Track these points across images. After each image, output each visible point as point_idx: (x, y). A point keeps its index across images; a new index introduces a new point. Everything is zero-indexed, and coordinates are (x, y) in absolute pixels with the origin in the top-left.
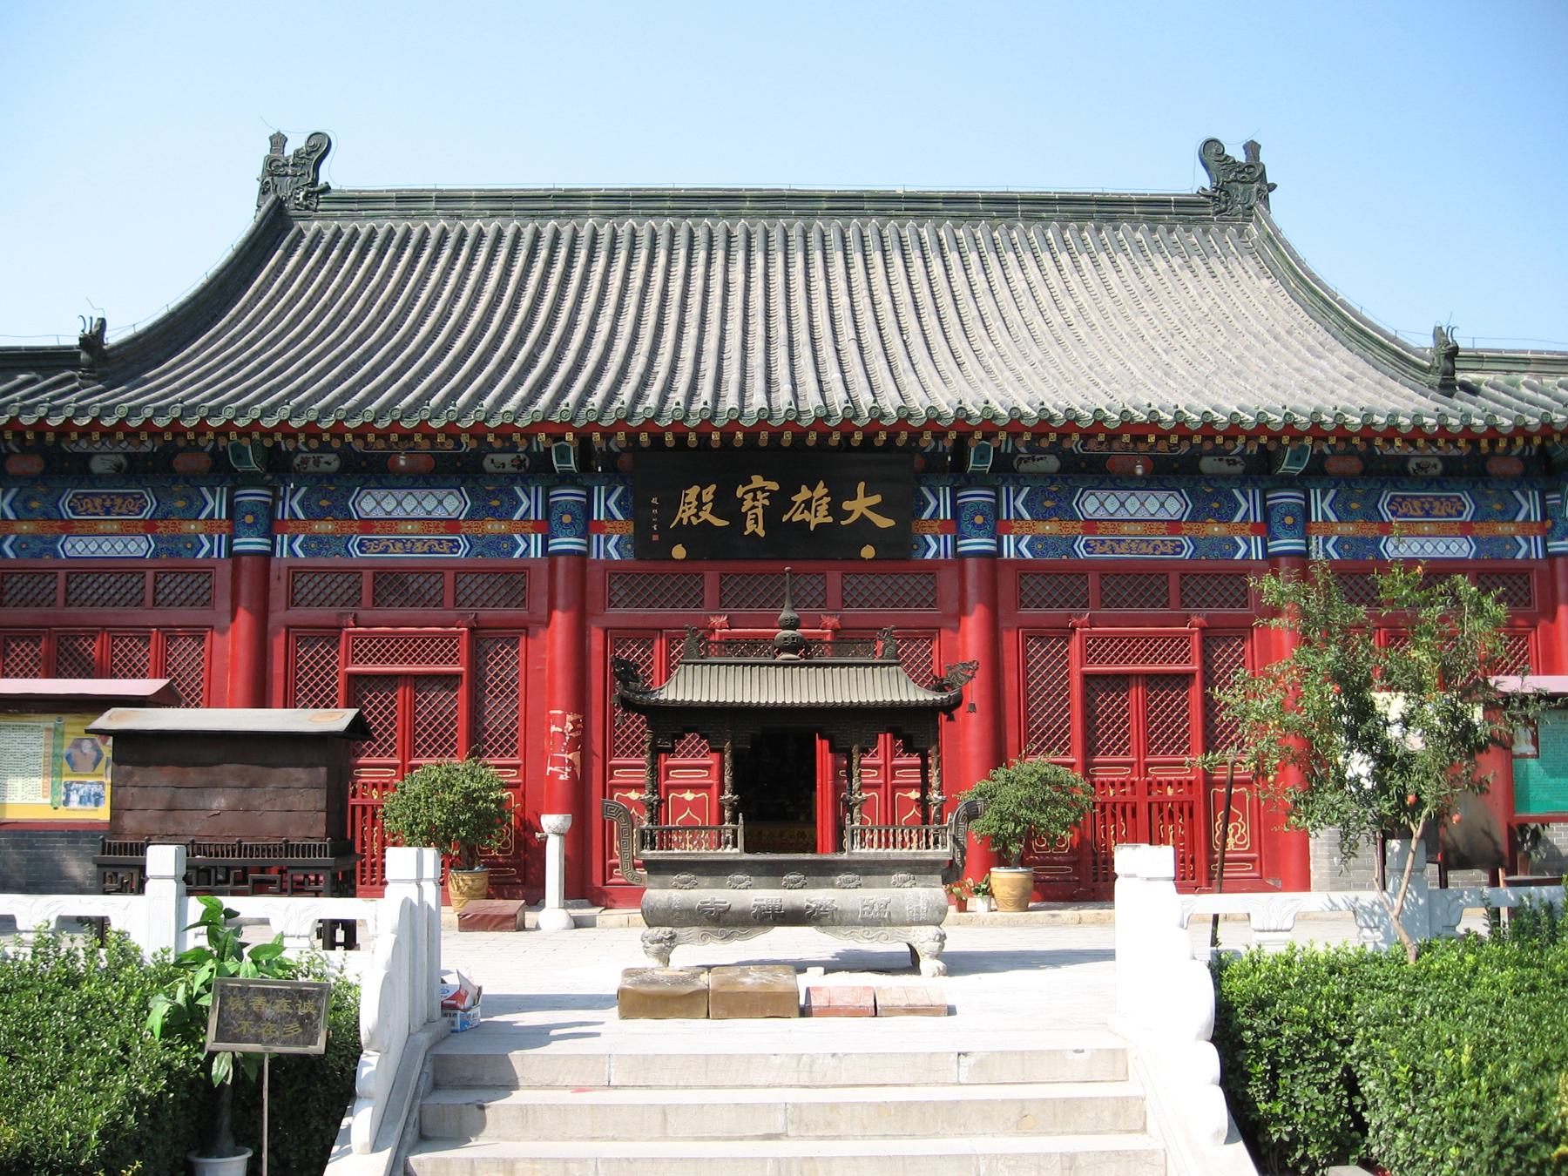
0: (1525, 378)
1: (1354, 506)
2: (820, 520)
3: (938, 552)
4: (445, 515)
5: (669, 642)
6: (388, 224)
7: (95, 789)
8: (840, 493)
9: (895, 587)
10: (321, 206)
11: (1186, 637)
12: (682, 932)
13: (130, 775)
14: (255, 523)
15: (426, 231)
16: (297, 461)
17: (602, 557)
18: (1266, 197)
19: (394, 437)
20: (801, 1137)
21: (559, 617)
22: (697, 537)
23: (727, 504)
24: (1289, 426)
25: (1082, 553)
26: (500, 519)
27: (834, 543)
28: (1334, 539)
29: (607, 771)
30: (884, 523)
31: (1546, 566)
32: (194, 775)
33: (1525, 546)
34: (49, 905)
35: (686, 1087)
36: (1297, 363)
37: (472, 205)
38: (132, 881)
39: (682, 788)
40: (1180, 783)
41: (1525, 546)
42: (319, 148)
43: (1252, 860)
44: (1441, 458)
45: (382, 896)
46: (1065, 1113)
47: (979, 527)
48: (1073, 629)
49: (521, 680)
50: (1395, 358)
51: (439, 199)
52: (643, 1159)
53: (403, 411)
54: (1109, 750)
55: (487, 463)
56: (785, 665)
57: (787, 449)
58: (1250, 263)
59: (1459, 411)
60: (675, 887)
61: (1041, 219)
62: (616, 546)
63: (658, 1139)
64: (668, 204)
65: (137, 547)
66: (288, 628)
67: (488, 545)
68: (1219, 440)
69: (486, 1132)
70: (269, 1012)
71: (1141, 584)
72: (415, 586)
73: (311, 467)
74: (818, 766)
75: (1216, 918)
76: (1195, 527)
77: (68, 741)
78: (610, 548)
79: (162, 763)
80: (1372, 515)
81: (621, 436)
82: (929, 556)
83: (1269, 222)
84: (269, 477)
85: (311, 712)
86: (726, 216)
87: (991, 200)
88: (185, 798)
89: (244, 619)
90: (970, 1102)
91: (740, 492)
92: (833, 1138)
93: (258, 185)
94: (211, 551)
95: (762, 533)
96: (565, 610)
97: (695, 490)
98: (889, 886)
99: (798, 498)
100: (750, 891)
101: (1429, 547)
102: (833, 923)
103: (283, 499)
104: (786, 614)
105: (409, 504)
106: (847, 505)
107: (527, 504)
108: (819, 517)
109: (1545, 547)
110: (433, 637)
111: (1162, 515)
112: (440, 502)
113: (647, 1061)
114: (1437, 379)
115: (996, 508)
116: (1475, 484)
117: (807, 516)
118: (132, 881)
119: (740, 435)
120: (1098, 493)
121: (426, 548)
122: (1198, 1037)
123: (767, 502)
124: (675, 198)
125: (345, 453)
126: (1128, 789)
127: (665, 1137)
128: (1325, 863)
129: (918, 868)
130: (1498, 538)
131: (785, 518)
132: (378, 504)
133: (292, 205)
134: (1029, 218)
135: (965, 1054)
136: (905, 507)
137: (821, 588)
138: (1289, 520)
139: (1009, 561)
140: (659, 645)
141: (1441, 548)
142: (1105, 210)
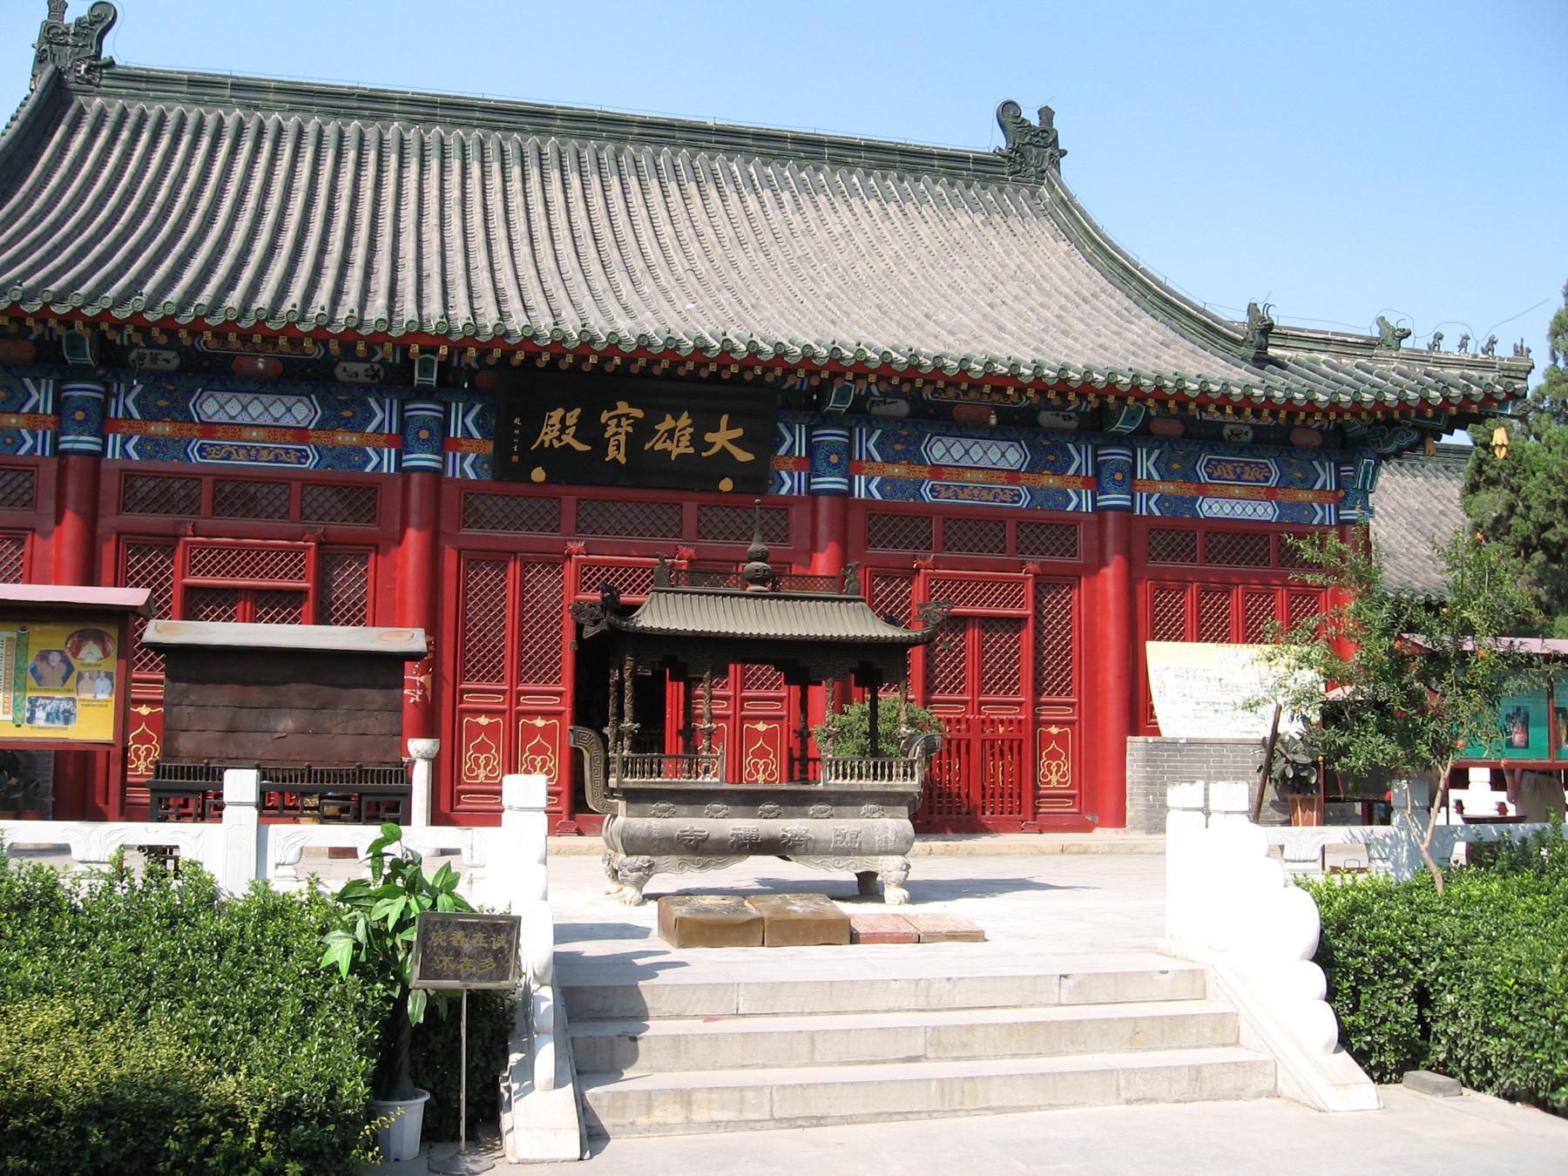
0: (1323, 357)
1: (1175, 466)
2: (682, 450)
3: (792, 488)
4: (293, 423)
5: (523, 565)
6: (179, 108)
7: (64, 705)
8: (704, 423)
9: (531, 511)
10: (104, 82)
11: (1020, 582)
12: (660, 860)
13: (186, 693)
14: (86, 420)
15: (221, 120)
16: (133, 355)
17: (458, 475)
19: (257, 338)
20: (939, 1059)
21: (412, 534)
22: (559, 462)
23: (590, 430)
24: (1136, 388)
25: (928, 497)
26: (352, 430)
27: (697, 474)
28: (1156, 496)
29: (458, 695)
30: (744, 456)
31: (1094, 518)
32: (257, 694)
33: (1320, 513)
34: (110, 833)
35: (811, 1014)
36: (1114, 328)
37: (271, 96)
38: (209, 808)
39: (534, 714)
40: (1011, 722)
41: (1320, 513)
43: (1072, 797)
44: (1252, 426)
45: (499, 824)
46: (1170, 1030)
48: (918, 570)
49: (369, 599)
50: (1208, 331)
52: (816, 1085)
53: (55, 294)
54: (946, 688)
55: (339, 371)
56: (756, 597)
57: (515, 368)
58: (1048, 224)
59: (1279, 385)
60: (653, 815)
61: (846, 164)
62: (473, 465)
63: (806, 1065)
64: (478, 115)
65: (1264, 511)
66: (119, 534)
67: (338, 457)
68: (895, 381)
69: (638, 1063)
70: (467, 947)
71: (885, 524)
72: (145, 489)
73: (147, 364)
74: (668, 696)
75: (1323, 848)
76: (1032, 477)
77: (33, 654)
78: (466, 467)
79: (222, 681)
80: (1190, 476)
81: (472, 352)
82: (784, 491)
83: (1062, 186)
84: (101, 372)
85: (285, 627)
86: (537, 133)
87: (800, 140)
88: (247, 718)
89: (70, 520)
90: (1090, 1021)
91: (604, 417)
92: (968, 1058)
93: (33, 52)
94: (34, 448)
95: (623, 460)
96: (420, 528)
97: (559, 412)
98: (858, 816)
99: (662, 427)
100: (727, 821)
101: (1238, 509)
102: (807, 852)
103: (117, 396)
104: (756, 546)
105: (256, 409)
106: (709, 437)
107: (381, 416)
108: (681, 447)
109: (1337, 515)
110: (279, 550)
111: (1003, 465)
112: (289, 410)
113: (774, 988)
114: (1252, 353)
116: (1281, 453)
117: (669, 446)
118: (209, 808)
119: (617, 360)
120: (945, 439)
121: (271, 457)
122: (1302, 958)
123: (630, 429)
124: (484, 109)
125: (914, 399)
126: (964, 726)
127: (813, 1063)
128: (1142, 801)
129: (887, 800)
130: (1299, 504)
131: (647, 446)
132: (222, 407)
133: (71, 78)
134: (836, 162)
135: (1065, 976)
136: (763, 441)
137: (284, 497)
138: (1118, 476)
139: (860, 501)
140: (514, 568)
141: (1249, 510)
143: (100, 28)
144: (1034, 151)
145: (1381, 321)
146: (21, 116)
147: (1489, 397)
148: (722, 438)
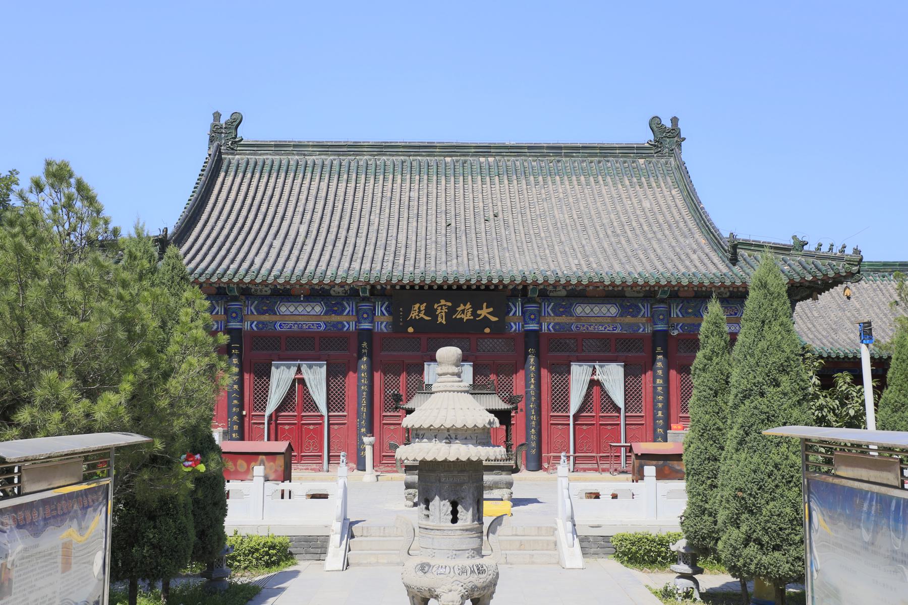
8: (476, 307)
18: (680, 145)
23: (430, 311)
26: (338, 314)
42: (236, 121)
47: (533, 320)
51: (295, 146)
95: (444, 322)
97: (417, 305)
106: (479, 312)
108: (467, 316)
115: (539, 312)
117: (462, 316)
124: (404, 147)
139: (545, 333)
142: (604, 151)
143: (235, 124)
144: (668, 140)
145: (794, 237)
146: (207, 169)
147: (838, 274)
148: (484, 312)
